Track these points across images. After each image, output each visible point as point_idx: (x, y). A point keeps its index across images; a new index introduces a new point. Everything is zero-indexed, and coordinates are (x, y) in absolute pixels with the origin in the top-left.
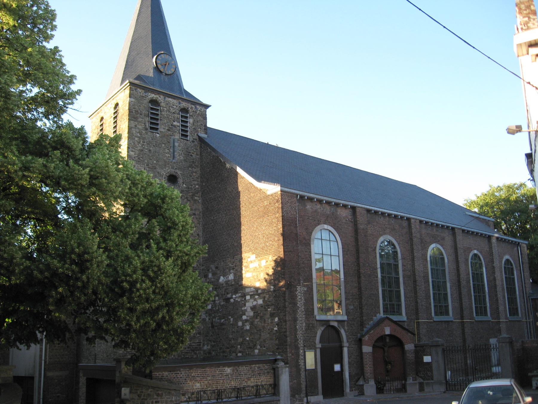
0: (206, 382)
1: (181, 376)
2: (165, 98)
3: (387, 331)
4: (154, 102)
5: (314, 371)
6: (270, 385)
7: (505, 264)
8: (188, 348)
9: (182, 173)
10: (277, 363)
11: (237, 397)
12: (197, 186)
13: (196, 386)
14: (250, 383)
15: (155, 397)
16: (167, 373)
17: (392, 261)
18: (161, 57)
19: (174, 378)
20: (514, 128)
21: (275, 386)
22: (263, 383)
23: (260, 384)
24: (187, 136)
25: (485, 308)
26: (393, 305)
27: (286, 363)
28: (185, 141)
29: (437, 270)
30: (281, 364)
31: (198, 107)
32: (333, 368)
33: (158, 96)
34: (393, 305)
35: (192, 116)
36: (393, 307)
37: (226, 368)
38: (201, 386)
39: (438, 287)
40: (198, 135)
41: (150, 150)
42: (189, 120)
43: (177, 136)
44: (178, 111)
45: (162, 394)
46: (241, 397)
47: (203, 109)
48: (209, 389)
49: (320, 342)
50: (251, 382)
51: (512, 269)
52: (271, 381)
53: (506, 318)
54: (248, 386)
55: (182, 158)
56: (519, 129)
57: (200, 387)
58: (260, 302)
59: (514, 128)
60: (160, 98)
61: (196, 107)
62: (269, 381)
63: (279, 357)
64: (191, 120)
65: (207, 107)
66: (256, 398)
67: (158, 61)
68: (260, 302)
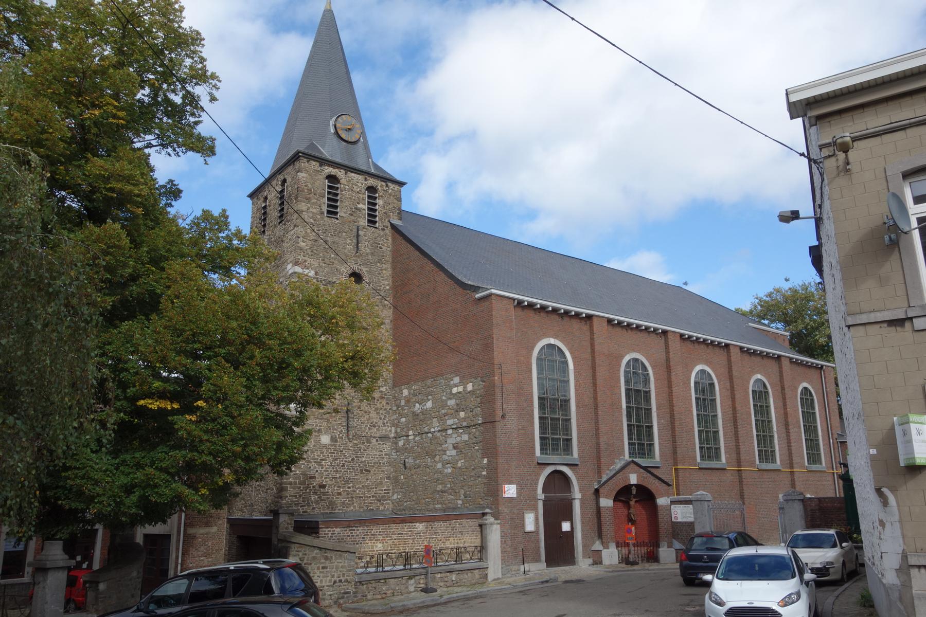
0: (390, 542)
3: (633, 479)
5: (536, 532)
6: (476, 547)
7: (802, 394)
11: (456, 561)
14: (448, 545)
15: (323, 561)
16: (338, 529)
17: (641, 387)
20: (789, 214)
21: (482, 549)
22: (466, 545)
24: (375, 222)
25: (773, 452)
26: (643, 444)
27: (496, 519)
28: (373, 229)
29: (704, 400)
30: (490, 519)
31: (389, 184)
32: (560, 527)
33: (337, 170)
37: (418, 524)
39: (706, 422)
42: (377, 201)
43: (364, 222)
44: (363, 190)
47: (397, 187)
49: (544, 492)
51: (812, 400)
52: (478, 542)
53: (803, 466)
54: (447, 549)
55: (368, 251)
56: (795, 215)
58: (465, 437)
59: (789, 214)
60: (340, 173)
63: (487, 510)
64: (380, 202)
65: (401, 184)
67: (338, 125)
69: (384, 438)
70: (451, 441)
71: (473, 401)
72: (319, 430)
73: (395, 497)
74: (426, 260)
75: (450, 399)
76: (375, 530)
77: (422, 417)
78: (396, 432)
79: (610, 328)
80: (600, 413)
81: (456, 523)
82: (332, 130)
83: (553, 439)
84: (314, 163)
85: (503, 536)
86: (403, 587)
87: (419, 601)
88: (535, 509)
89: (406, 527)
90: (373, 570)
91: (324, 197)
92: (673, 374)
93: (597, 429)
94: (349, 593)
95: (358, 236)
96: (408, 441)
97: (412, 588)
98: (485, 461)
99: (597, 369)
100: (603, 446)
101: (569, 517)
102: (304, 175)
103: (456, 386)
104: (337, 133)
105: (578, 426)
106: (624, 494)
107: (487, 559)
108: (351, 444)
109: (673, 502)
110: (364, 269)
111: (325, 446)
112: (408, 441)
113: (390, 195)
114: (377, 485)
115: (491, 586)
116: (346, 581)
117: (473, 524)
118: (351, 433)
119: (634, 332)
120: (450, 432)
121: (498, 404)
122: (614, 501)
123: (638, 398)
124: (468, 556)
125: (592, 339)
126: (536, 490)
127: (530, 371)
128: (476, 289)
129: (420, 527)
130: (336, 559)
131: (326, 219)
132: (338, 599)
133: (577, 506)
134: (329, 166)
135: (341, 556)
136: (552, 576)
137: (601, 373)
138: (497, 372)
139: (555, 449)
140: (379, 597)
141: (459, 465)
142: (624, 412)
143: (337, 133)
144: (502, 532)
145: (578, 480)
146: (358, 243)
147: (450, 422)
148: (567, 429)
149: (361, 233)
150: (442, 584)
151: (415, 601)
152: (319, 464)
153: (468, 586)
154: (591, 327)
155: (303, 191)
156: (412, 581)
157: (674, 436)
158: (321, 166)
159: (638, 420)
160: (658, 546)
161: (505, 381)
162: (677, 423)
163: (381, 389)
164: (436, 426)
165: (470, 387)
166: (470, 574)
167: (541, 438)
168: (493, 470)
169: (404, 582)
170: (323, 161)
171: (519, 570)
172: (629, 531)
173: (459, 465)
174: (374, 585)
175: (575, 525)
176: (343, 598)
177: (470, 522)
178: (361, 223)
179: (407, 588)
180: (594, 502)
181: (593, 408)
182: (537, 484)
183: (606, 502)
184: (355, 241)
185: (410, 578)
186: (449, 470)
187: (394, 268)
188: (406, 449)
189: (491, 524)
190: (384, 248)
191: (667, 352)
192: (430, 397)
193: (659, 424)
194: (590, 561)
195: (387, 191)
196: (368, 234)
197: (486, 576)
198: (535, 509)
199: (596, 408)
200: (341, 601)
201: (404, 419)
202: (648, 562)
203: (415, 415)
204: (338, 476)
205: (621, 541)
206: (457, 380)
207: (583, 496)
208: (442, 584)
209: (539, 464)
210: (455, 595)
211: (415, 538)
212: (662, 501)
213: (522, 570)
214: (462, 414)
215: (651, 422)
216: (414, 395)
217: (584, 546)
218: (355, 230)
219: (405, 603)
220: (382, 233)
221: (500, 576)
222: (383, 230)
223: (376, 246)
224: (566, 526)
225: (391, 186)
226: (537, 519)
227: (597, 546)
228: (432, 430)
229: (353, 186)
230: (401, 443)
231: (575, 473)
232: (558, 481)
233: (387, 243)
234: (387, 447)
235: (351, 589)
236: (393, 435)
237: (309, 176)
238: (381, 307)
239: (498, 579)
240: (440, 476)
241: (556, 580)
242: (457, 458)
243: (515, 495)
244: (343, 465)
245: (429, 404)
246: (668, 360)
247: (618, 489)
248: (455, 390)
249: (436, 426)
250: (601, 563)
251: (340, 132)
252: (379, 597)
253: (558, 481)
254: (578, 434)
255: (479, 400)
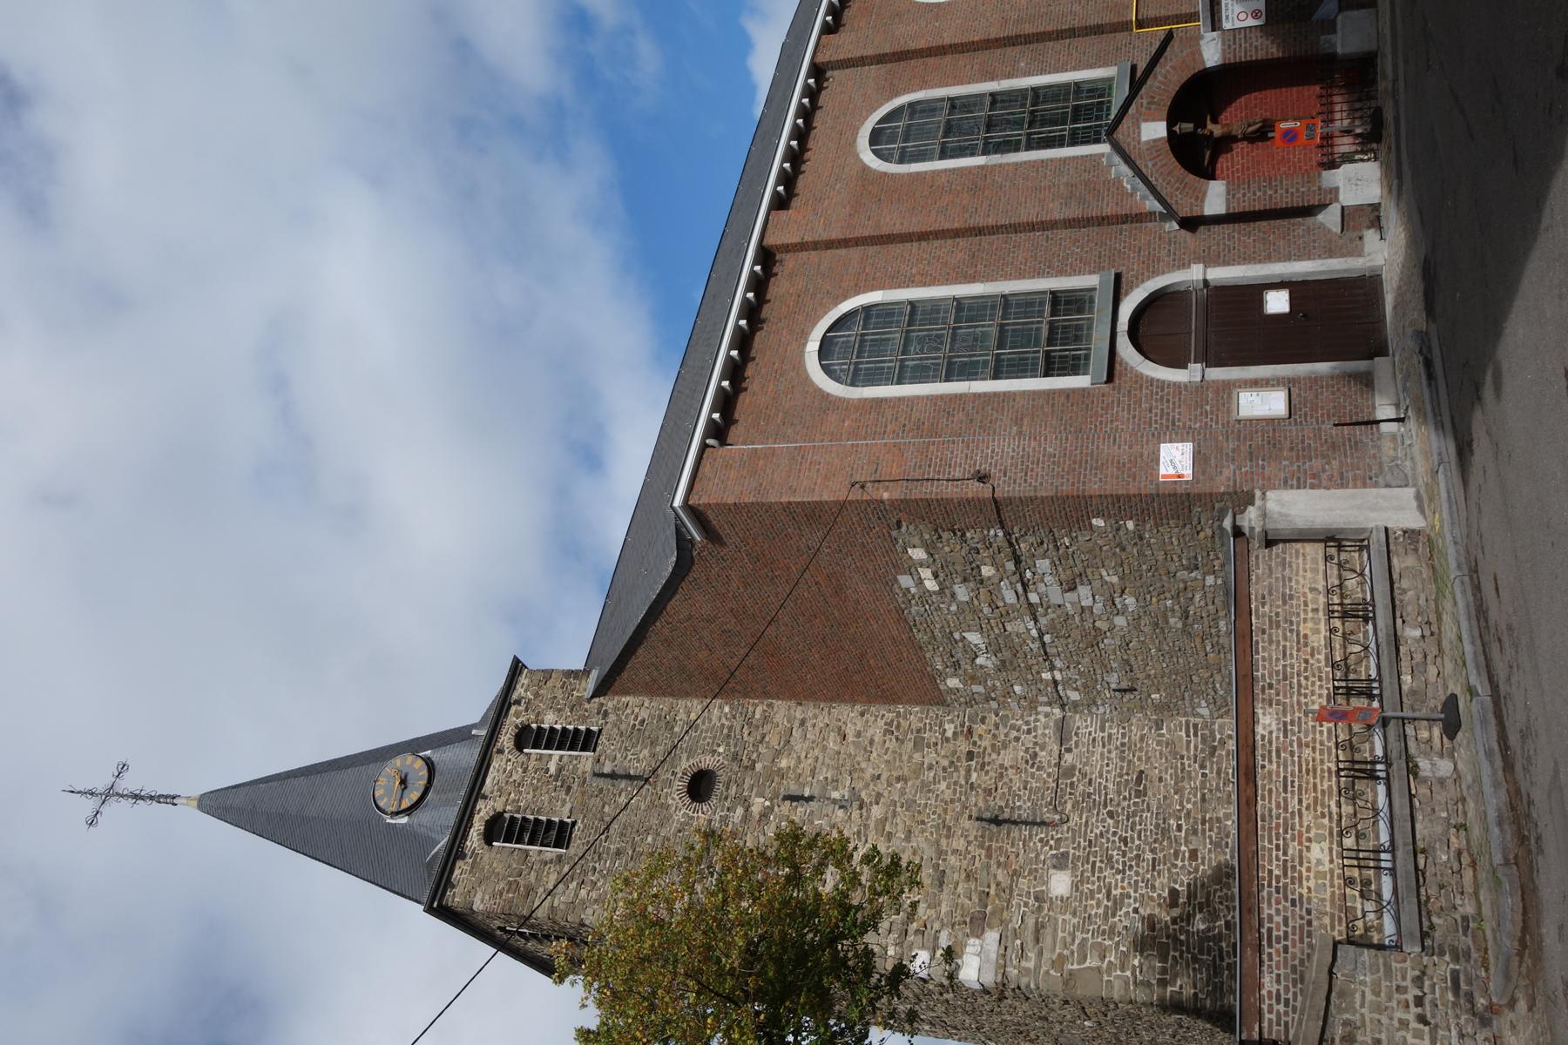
0: (1308, 818)
1: (1277, 919)
2: (485, 797)
3: (1155, 130)
4: (489, 836)
5: (1289, 384)
6: (1327, 558)
8: (1202, 767)
9: (685, 756)
10: (1247, 531)
11: (1361, 549)
12: (727, 709)
13: (1319, 862)
14: (1318, 640)
16: (1267, 980)
18: (382, 797)
19: (1286, 949)
21: (1332, 539)
22: (1321, 586)
23: (1322, 599)
27: (1249, 500)
28: (603, 739)
30: (1250, 518)
31: (515, 697)
33: (476, 818)
34: (1076, 109)
35: (538, 714)
36: (1080, 115)
37: (1259, 730)
38: (1320, 839)
40: (589, 700)
41: (618, 853)
44: (522, 758)
45: (1346, 1023)
46: (1370, 680)
47: (523, 680)
48: (1334, 809)
49: (1180, 364)
50: (1317, 632)
52: (1314, 551)
54: (1330, 644)
55: (646, 752)
57: (1326, 845)
58: (1043, 565)
61: (518, 702)
62: (1315, 561)
63: (1227, 523)
64: (550, 720)
65: (517, 668)
66: (1374, 618)
67: (394, 809)
68: (1043, 565)
69: (1063, 732)
70: (1055, 595)
71: (949, 546)
72: (1037, 899)
73: (1205, 712)
74: (652, 637)
75: (953, 595)
76: (1271, 866)
77: (1007, 654)
78: (1050, 704)
79: (795, 203)
80: (991, 221)
81: (1261, 615)
82: (404, 820)
83: (1050, 342)
84: (457, 872)
85: (1298, 482)
86: (1441, 796)
87: (1486, 770)
88: (1228, 388)
89: (1268, 767)
90: (1387, 883)
91: (527, 852)
92: (913, 46)
93: (1032, 227)
94: (1455, 977)
95: (613, 776)
96: (1067, 682)
97: (1445, 767)
98: (1098, 522)
99: (885, 231)
100: (1074, 212)
101: (1254, 293)
102: (479, 895)
103: (920, 582)
104: (409, 811)
105: (1021, 275)
106: (1195, 153)
107: (1364, 530)
108: (1075, 818)
109: (1215, 24)
110: (684, 764)
111: (1076, 886)
112: (1067, 682)
113: (537, 695)
114: (1175, 754)
115: (1440, 522)
116: (1418, 981)
117: (1262, 563)
118: (1048, 817)
119: (811, 144)
120: (1034, 598)
121: (950, 491)
122: (1213, 178)
123: (962, 127)
124: (1352, 583)
125: (816, 246)
126: (1177, 385)
127: (879, 402)
128: (683, 544)
129: (1267, 722)
130: (1351, 1008)
131: (572, 850)
132: (1473, 1012)
133: (1221, 274)
134: (465, 837)
135: (1342, 994)
136: (1411, 344)
137: (893, 222)
138: (873, 492)
139: (1077, 334)
140: (1468, 874)
141: (1115, 579)
142: (996, 159)
143: (409, 811)
144: (1286, 484)
145: (1156, 273)
146: (628, 777)
147: (1010, 597)
148: (1027, 303)
149: (607, 769)
150: (1432, 671)
151: (1486, 780)
152: (1118, 903)
153: (1440, 593)
154: (788, 248)
155: (511, 901)
156: (1424, 764)
157: (1059, 35)
158: (463, 857)
159: (1018, 124)
160: (1332, 58)
161: (896, 472)
162: (1028, 29)
163: (949, 734)
164: (1024, 627)
165: (918, 554)
166: (1405, 584)
167: (1046, 375)
168: (1118, 506)
169: (1423, 791)
170: (455, 850)
171: (1393, 437)
172: (1290, 136)
173: (1115, 579)
174: (1433, 891)
175: (1275, 276)
176: (1470, 997)
177: (1259, 571)
178: (588, 767)
179: (1442, 782)
180: (1216, 229)
181: (977, 238)
182: (1162, 384)
183: (1215, 198)
184: (623, 784)
185: (1413, 770)
186: (1130, 600)
187: (687, 694)
188: (1085, 686)
189: (1264, 515)
190: (644, 714)
191: (861, 62)
192: (957, 636)
193: (1028, 74)
194: (1371, 236)
195: (528, 703)
196: (611, 753)
197: (1411, 534)
198: (1228, 388)
199: (979, 231)
200: (1481, 1002)
201: (1017, 688)
202: (1374, 81)
203: (1002, 666)
204: (1149, 856)
205: (1317, 157)
206: (905, 581)
207: (1198, 260)
208: (1432, 671)
209: (1110, 378)
210: (1468, 648)
211: (1297, 734)
212: (1212, 53)
213: (1393, 427)
214: (987, 571)
215: (1022, 93)
216: (956, 665)
217: (1331, 253)
218: (601, 782)
219: (1492, 815)
220: (612, 718)
221: (1409, 492)
222: (606, 714)
223: (637, 734)
224: (1278, 302)
225: (519, 691)
226: (1255, 384)
227: (1330, 218)
228: (1034, 633)
229: (513, 783)
230: (1074, 696)
231: (1140, 279)
232: (1159, 326)
233: (636, 707)
234: (1084, 725)
235: (1444, 967)
236: (1057, 711)
237: (484, 878)
238: (767, 728)
239: (1418, 497)
240: (1145, 620)
241: (1422, 338)
242: (1097, 584)
243: (1189, 446)
244: (1124, 840)
245: (974, 638)
246: (880, 59)
247: (1180, 171)
248: (931, 585)
249: (1024, 627)
250: (1375, 207)
251: (406, 804)
252: (1468, 874)
253: (1159, 326)
254: (1040, 274)
255: (945, 535)
